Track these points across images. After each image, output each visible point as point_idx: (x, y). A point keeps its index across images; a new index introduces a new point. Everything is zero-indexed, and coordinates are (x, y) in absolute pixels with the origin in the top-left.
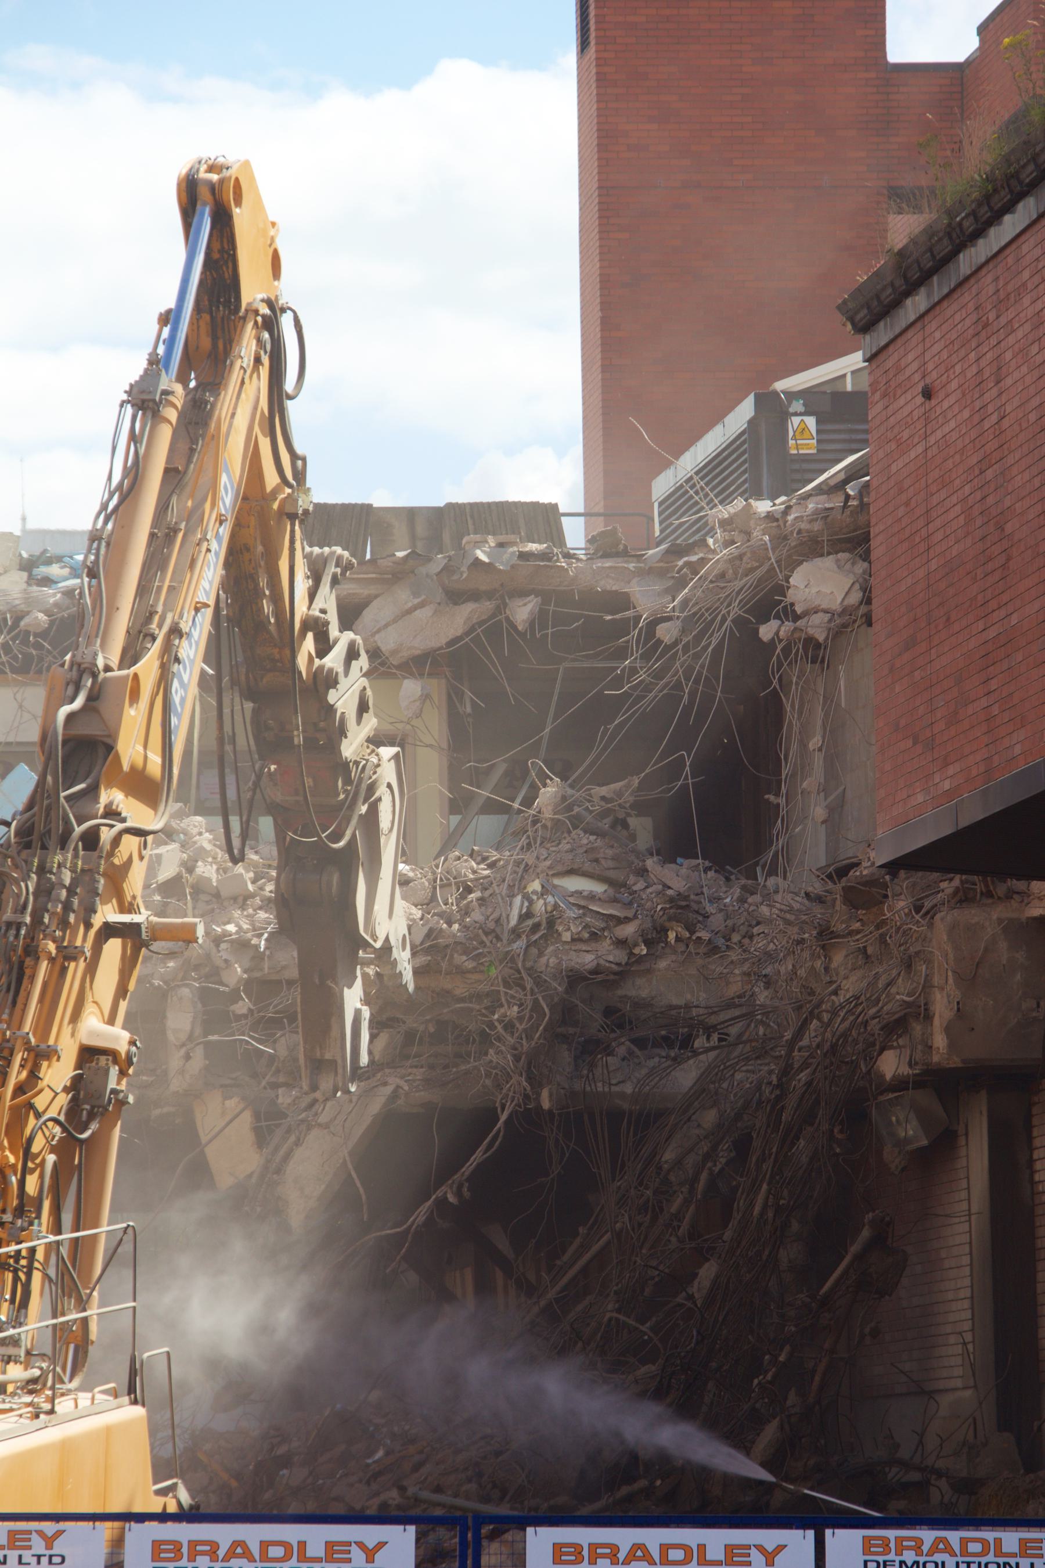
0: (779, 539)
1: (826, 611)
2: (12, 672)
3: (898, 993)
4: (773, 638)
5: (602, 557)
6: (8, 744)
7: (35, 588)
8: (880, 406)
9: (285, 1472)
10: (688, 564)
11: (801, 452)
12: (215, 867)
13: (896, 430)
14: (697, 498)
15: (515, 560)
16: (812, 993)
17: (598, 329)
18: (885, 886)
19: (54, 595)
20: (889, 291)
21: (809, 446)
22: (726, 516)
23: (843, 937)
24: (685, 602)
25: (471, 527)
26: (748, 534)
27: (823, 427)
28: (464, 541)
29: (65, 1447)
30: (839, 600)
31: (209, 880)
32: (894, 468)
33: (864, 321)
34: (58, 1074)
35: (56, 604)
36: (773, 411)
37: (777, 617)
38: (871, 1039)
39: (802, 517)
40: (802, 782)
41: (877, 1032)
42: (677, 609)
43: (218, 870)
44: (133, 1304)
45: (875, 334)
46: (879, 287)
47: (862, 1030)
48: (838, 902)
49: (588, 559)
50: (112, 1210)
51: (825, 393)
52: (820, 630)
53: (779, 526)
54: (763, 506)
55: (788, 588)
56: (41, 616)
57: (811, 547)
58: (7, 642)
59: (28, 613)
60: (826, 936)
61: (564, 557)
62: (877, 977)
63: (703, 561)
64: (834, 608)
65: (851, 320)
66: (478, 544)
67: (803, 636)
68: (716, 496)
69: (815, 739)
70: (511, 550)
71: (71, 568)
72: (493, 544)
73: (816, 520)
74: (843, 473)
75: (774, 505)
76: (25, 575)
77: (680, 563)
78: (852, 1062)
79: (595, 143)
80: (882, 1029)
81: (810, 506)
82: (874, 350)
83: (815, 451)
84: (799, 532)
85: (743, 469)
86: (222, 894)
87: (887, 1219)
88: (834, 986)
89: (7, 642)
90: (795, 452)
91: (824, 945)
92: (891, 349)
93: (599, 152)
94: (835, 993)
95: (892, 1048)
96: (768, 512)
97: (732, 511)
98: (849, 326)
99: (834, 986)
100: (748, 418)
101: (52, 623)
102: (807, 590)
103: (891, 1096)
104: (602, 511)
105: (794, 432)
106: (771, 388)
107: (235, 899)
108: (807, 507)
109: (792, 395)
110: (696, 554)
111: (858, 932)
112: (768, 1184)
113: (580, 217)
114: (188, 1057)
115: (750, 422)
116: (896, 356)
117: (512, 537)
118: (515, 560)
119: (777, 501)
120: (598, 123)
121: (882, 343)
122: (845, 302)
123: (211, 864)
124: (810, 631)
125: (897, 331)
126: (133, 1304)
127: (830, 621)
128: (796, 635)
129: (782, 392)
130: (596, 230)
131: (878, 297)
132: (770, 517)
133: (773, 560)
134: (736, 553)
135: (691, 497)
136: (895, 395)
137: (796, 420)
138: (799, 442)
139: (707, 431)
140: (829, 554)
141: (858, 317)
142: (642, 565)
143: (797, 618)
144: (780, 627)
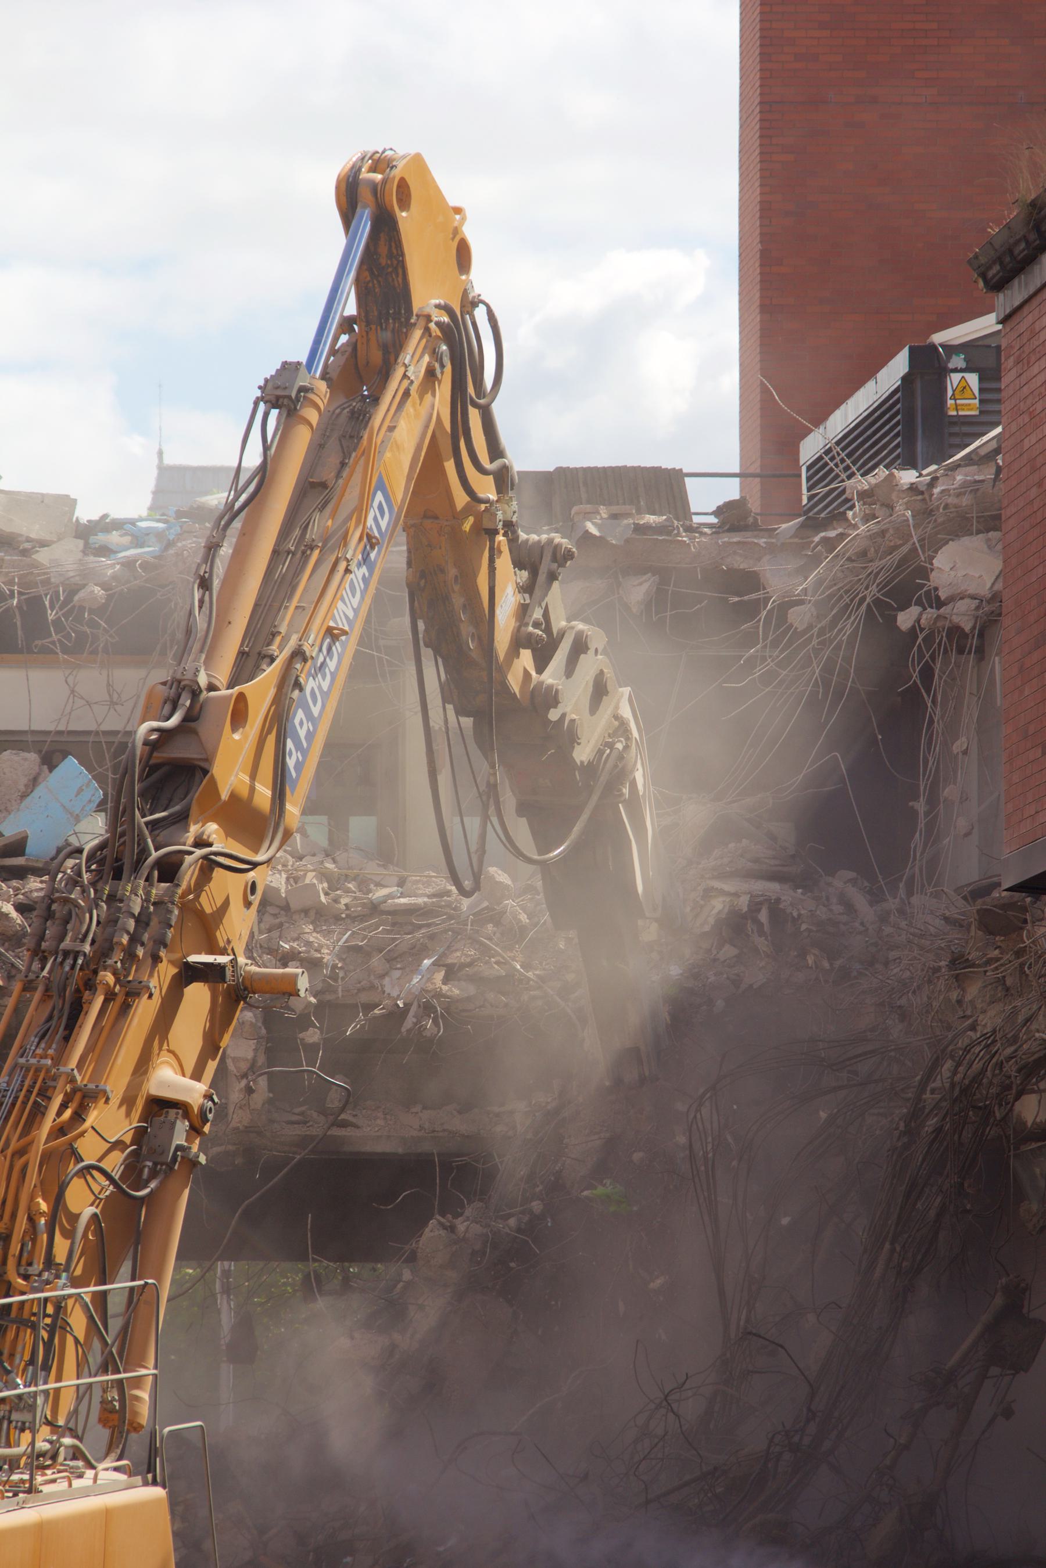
0: (925, 513)
1: (973, 597)
2: (64, 652)
3: (1038, 1031)
4: (914, 627)
5: (729, 530)
6: (60, 733)
7: (92, 558)
8: (1013, 374)
9: (349, 1559)
10: (825, 540)
11: (961, 413)
12: (284, 876)
13: (1029, 401)
14: (848, 462)
15: (629, 534)
16: (949, 1028)
17: (757, 264)
18: (1024, 909)
19: (112, 566)
20: (1023, 245)
21: (969, 407)
22: (866, 488)
23: (979, 966)
24: (819, 582)
25: (584, 496)
26: (891, 507)
27: (987, 385)
28: (573, 512)
29: (41, 1530)
30: (989, 585)
31: (278, 890)
32: (1027, 443)
33: (997, 278)
34: (109, 1125)
35: (114, 577)
36: (929, 365)
37: (919, 603)
38: (1007, 1082)
39: (948, 490)
40: (944, 789)
41: (1014, 1074)
42: (810, 592)
43: (288, 879)
44: (155, 1372)
45: (1008, 292)
46: (1012, 241)
47: (997, 1072)
48: (973, 927)
49: (713, 533)
50: (178, 1258)
51: (989, 346)
52: (966, 618)
53: (924, 500)
54: (908, 477)
55: (932, 570)
56: (97, 589)
57: (960, 525)
58: (59, 618)
59: (84, 586)
60: (959, 962)
61: (686, 531)
62: (1015, 1012)
63: (842, 536)
64: (983, 594)
65: (983, 276)
66: (588, 516)
67: (947, 624)
68: (854, 463)
69: (958, 743)
70: (625, 522)
71: (132, 535)
72: (605, 516)
73: (964, 493)
74: (995, 442)
75: (921, 475)
76: (81, 543)
77: (817, 539)
78: (986, 1106)
79: (758, 52)
80: (1019, 1071)
81: (959, 478)
82: (1008, 311)
83: (976, 413)
84: (946, 507)
85: (895, 431)
86: (291, 906)
87: (1023, 1285)
88: (970, 1021)
89: (59, 618)
90: (955, 413)
91: (957, 976)
92: (1026, 310)
93: (761, 62)
94: (973, 1028)
95: (1033, 1092)
96: (912, 484)
97: (873, 481)
98: (981, 284)
99: (970, 1021)
100: (902, 374)
101: (109, 598)
102: (952, 573)
103: (1034, 1145)
104: (758, 471)
105: (954, 391)
106: (928, 341)
107: (306, 912)
108: (954, 479)
109: (951, 349)
110: (835, 529)
111: (997, 960)
112: (892, 1244)
113: (740, 136)
114: (249, 1091)
115: (904, 379)
116: (1030, 318)
117: (627, 508)
118: (629, 534)
119: (924, 472)
120: (761, 29)
121: (1017, 303)
122: (976, 257)
123: (280, 872)
124: (956, 619)
125: (1032, 290)
126: (155, 1372)
127: (978, 608)
128: (939, 624)
129: (941, 345)
130: (757, 152)
131: (1010, 251)
132: (913, 488)
133: (915, 539)
134: (876, 529)
135: (826, 464)
136: (1028, 363)
137: (956, 377)
138: (958, 402)
139: (858, 389)
140: (979, 532)
141: (991, 273)
142: (774, 540)
143: (940, 604)
144: (921, 614)
